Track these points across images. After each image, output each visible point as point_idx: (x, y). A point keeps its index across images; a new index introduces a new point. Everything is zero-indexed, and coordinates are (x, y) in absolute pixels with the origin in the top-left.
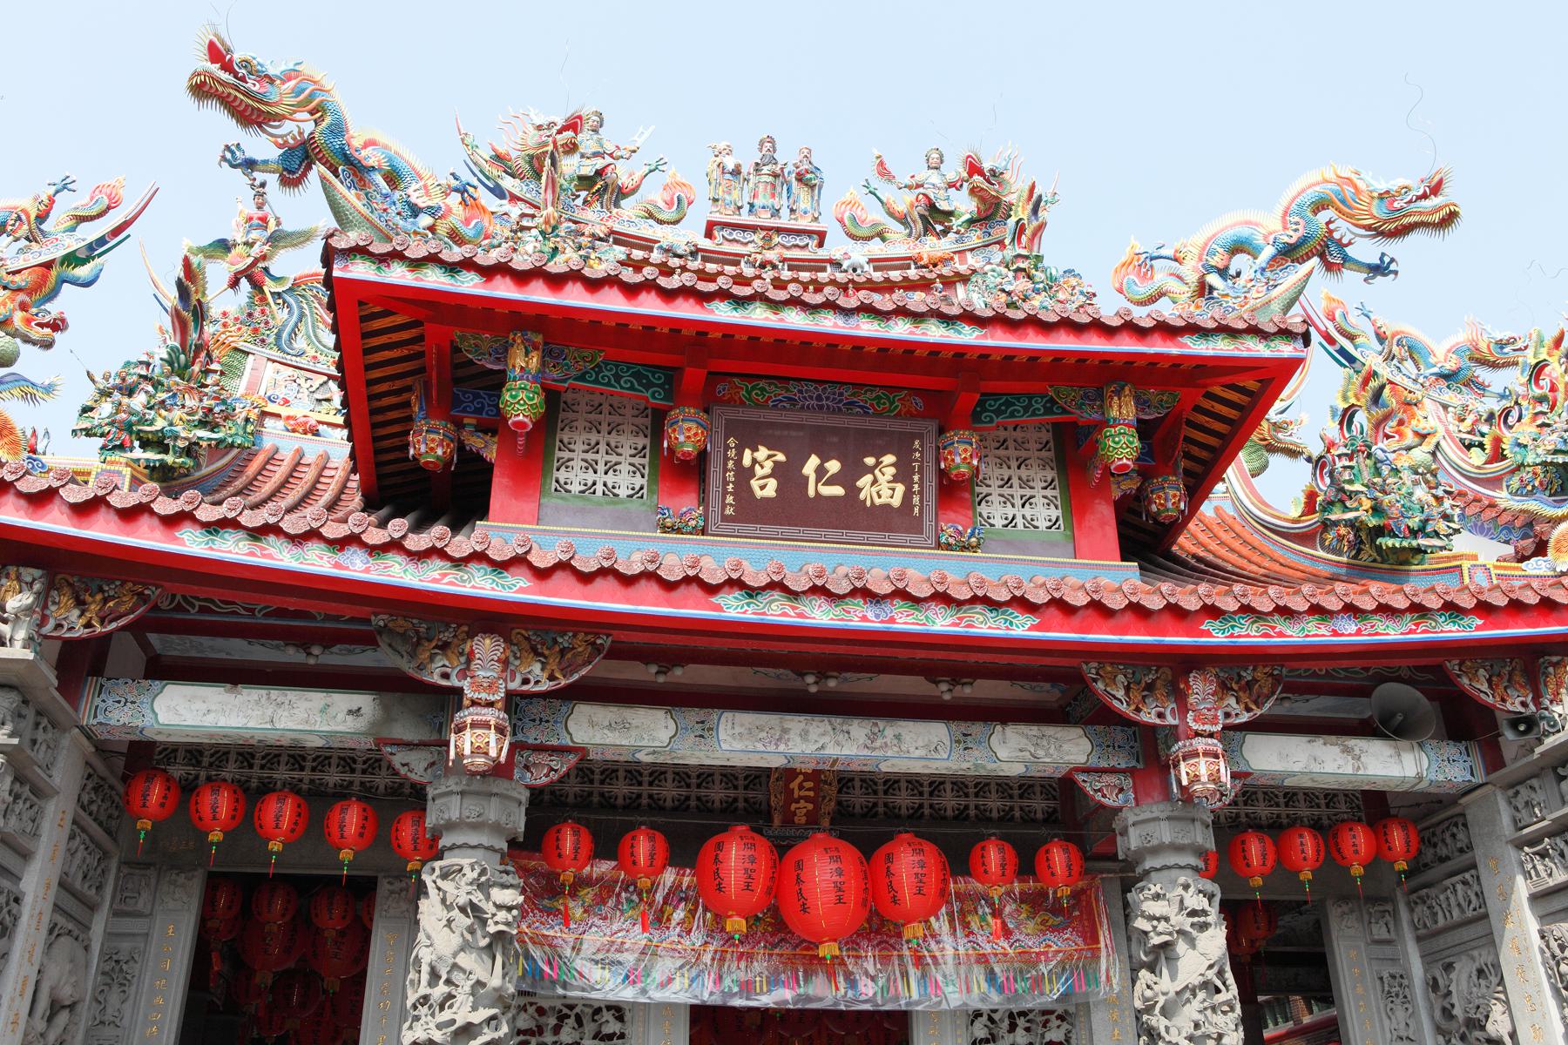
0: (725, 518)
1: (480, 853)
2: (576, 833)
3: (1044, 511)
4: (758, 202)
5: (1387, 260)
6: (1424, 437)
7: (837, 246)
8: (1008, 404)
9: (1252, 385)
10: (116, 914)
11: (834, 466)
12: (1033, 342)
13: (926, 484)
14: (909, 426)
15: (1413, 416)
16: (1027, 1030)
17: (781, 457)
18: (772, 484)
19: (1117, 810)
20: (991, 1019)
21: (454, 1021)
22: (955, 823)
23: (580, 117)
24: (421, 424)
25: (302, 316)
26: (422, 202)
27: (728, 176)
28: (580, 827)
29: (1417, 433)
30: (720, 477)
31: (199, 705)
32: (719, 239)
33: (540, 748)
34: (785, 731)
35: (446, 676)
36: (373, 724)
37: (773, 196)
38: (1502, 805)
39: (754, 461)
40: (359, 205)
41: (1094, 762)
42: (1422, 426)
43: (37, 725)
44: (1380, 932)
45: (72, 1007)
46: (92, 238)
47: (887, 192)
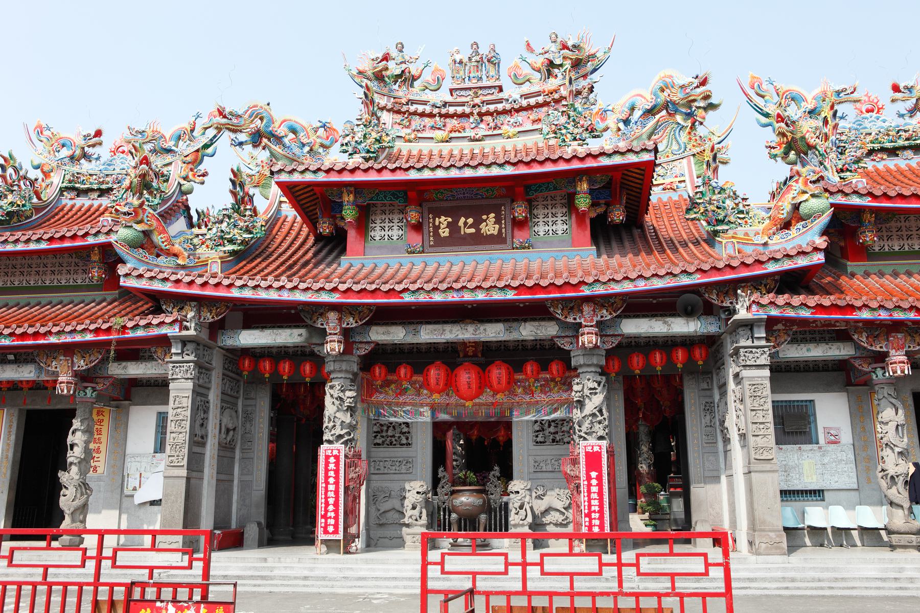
0: (430, 246)
2: (380, 368)
4: (472, 75)
8: (540, 187)
11: (470, 221)
12: (537, 169)
14: (498, 201)
17: (450, 220)
22: (514, 356)
26: (305, 141)
27: (457, 65)
28: (380, 368)
30: (428, 229)
32: (455, 96)
33: (361, 342)
34: (444, 330)
35: (322, 324)
36: (306, 339)
40: (280, 151)
41: (560, 334)
44: (705, 386)
45: (234, 429)
47: (531, 58)
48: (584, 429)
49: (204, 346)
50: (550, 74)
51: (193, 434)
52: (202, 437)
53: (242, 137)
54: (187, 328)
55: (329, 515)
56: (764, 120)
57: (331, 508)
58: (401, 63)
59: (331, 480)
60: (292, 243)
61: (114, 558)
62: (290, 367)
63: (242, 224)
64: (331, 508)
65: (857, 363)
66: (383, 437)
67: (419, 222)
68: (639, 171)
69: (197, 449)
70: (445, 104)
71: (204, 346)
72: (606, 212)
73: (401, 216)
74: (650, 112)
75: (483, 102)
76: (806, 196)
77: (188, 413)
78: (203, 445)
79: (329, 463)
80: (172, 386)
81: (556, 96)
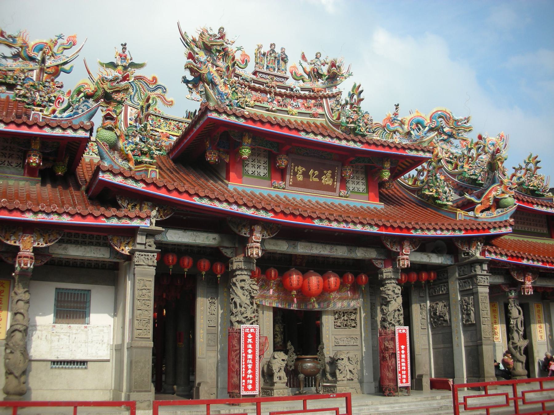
0: (290, 185)
3: (362, 187)
7: (290, 82)
11: (316, 173)
17: (304, 169)
19: (380, 268)
25: (137, 90)
31: (177, 235)
34: (312, 247)
35: (245, 234)
38: (457, 270)
44: (422, 295)
47: (305, 64)
55: (248, 376)
57: (250, 371)
59: (250, 351)
61: (508, 399)
64: (250, 371)
65: (503, 287)
79: (248, 338)
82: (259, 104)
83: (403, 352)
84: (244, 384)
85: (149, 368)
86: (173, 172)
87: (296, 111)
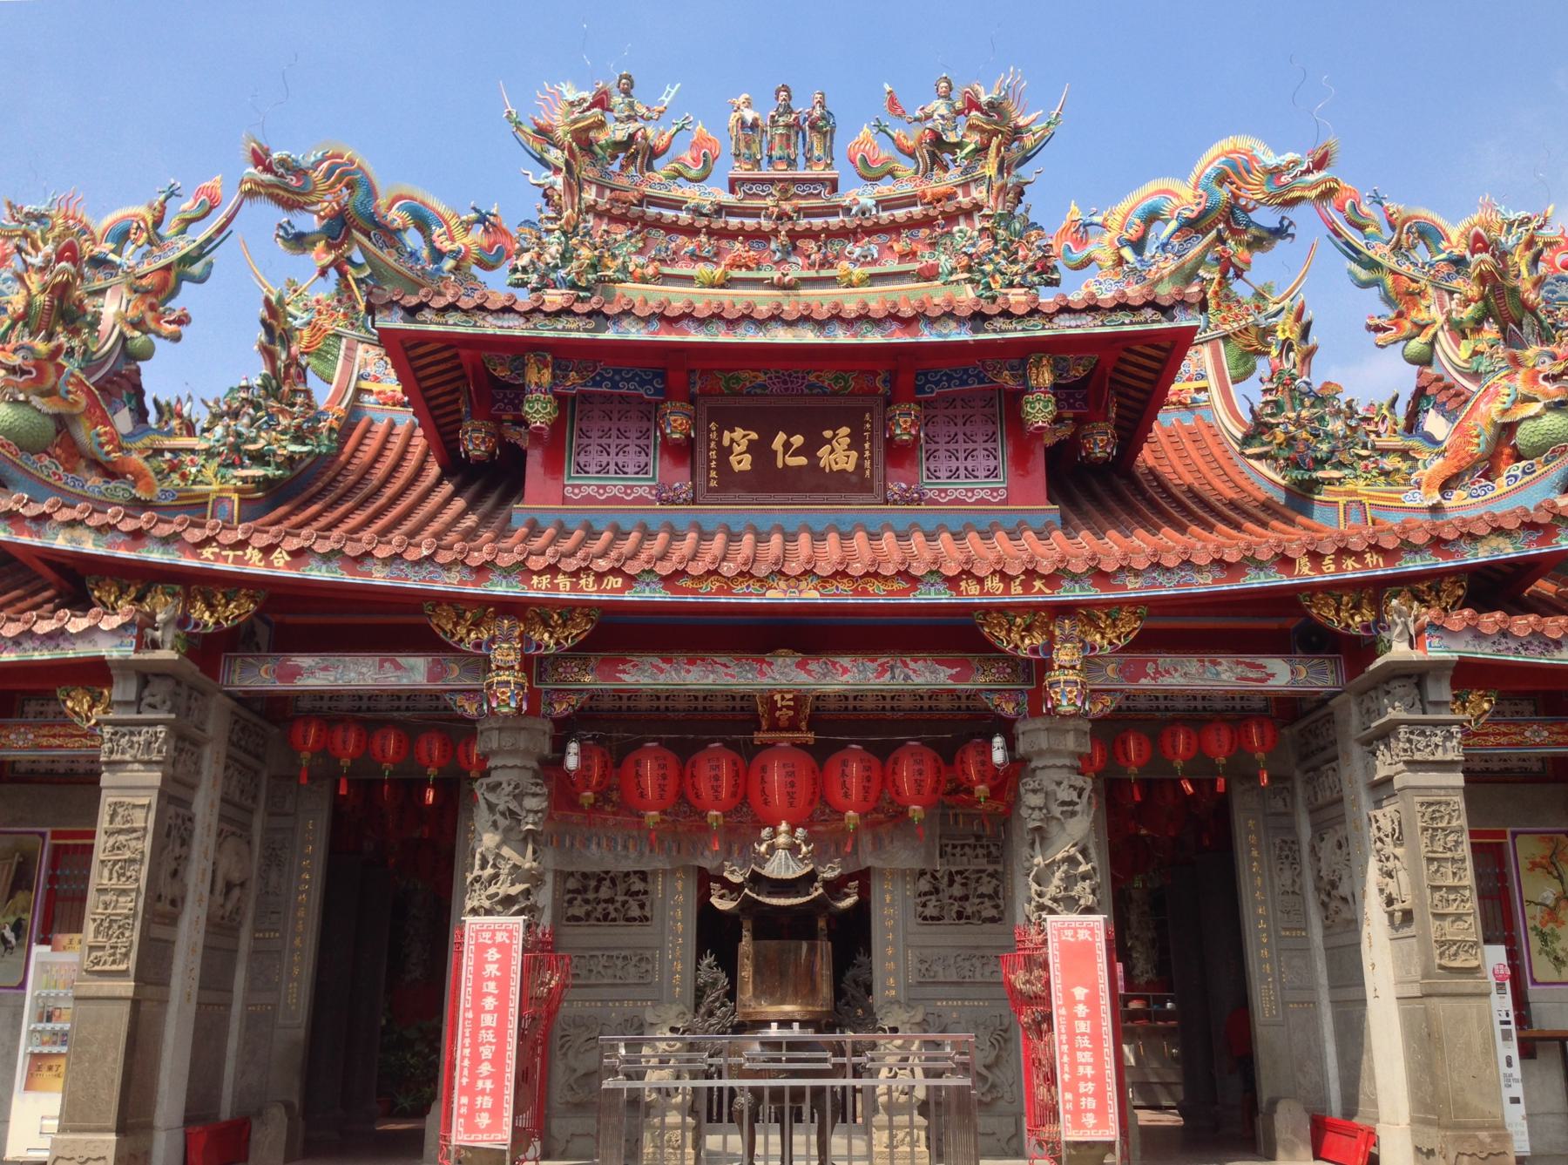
1: (516, 771)
5: (1286, 223)
6: (1424, 327)
9: (1166, 344)
10: (271, 814)
11: (798, 440)
13: (876, 450)
15: (1416, 305)
16: (963, 885)
17: (754, 436)
18: (748, 458)
20: (933, 876)
21: (497, 894)
23: (605, 93)
24: (468, 425)
26: (447, 246)
29: (1415, 324)
37: (788, 146)
39: (732, 441)
40: (391, 261)
42: (1423, 316)
43: (190, 697)
45: (242, 885)
46: (200, 239)
48: (1051, 890)
49: (191, 688)
50: (935, 160)
51: (154, 894)
52: (173, 903)
53: (309, 222)
54: (155, 645)
55: (480, 1084)
56: (1364, 275)
57: (485, 1068)
58: (629, 118)
59: (489, 1003)
60: (396, 467)
62: (399, 741)
63: (284, 421)
66: (587, 902)
67: (688, 436)
68: (1153, 352)
69: (158, 931)
70: (720, 210)
71: (191, 688)
72: (1074, 436)
73: (645, 425)
74: (1192, 226)
75: (798, 210)
76: (1534, 408)
77: (147, 845)
78: (172, 920)
79: (486, 961)
80: (106, 779)
81: (950, 207)
82: (743, 273)
83: (1081, 1010)
84: (464, 1110)
85: (115, 1060)
86: (1268, 519)
87: (858, 272)
